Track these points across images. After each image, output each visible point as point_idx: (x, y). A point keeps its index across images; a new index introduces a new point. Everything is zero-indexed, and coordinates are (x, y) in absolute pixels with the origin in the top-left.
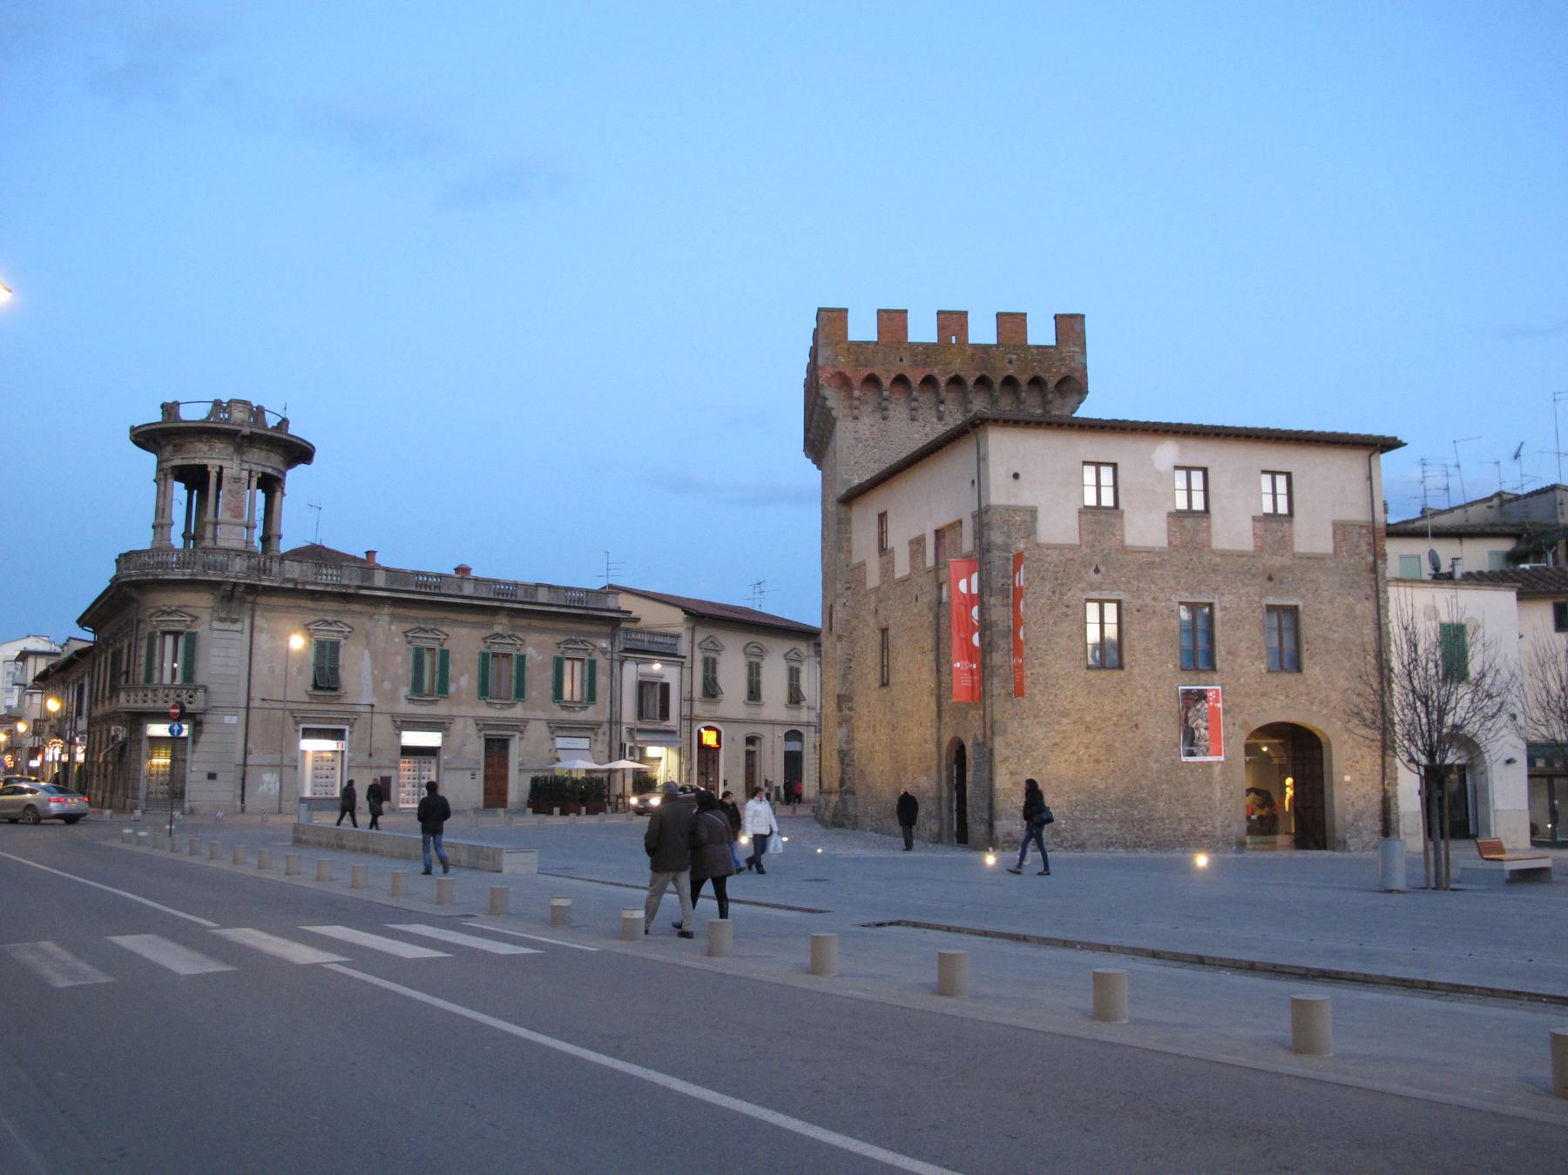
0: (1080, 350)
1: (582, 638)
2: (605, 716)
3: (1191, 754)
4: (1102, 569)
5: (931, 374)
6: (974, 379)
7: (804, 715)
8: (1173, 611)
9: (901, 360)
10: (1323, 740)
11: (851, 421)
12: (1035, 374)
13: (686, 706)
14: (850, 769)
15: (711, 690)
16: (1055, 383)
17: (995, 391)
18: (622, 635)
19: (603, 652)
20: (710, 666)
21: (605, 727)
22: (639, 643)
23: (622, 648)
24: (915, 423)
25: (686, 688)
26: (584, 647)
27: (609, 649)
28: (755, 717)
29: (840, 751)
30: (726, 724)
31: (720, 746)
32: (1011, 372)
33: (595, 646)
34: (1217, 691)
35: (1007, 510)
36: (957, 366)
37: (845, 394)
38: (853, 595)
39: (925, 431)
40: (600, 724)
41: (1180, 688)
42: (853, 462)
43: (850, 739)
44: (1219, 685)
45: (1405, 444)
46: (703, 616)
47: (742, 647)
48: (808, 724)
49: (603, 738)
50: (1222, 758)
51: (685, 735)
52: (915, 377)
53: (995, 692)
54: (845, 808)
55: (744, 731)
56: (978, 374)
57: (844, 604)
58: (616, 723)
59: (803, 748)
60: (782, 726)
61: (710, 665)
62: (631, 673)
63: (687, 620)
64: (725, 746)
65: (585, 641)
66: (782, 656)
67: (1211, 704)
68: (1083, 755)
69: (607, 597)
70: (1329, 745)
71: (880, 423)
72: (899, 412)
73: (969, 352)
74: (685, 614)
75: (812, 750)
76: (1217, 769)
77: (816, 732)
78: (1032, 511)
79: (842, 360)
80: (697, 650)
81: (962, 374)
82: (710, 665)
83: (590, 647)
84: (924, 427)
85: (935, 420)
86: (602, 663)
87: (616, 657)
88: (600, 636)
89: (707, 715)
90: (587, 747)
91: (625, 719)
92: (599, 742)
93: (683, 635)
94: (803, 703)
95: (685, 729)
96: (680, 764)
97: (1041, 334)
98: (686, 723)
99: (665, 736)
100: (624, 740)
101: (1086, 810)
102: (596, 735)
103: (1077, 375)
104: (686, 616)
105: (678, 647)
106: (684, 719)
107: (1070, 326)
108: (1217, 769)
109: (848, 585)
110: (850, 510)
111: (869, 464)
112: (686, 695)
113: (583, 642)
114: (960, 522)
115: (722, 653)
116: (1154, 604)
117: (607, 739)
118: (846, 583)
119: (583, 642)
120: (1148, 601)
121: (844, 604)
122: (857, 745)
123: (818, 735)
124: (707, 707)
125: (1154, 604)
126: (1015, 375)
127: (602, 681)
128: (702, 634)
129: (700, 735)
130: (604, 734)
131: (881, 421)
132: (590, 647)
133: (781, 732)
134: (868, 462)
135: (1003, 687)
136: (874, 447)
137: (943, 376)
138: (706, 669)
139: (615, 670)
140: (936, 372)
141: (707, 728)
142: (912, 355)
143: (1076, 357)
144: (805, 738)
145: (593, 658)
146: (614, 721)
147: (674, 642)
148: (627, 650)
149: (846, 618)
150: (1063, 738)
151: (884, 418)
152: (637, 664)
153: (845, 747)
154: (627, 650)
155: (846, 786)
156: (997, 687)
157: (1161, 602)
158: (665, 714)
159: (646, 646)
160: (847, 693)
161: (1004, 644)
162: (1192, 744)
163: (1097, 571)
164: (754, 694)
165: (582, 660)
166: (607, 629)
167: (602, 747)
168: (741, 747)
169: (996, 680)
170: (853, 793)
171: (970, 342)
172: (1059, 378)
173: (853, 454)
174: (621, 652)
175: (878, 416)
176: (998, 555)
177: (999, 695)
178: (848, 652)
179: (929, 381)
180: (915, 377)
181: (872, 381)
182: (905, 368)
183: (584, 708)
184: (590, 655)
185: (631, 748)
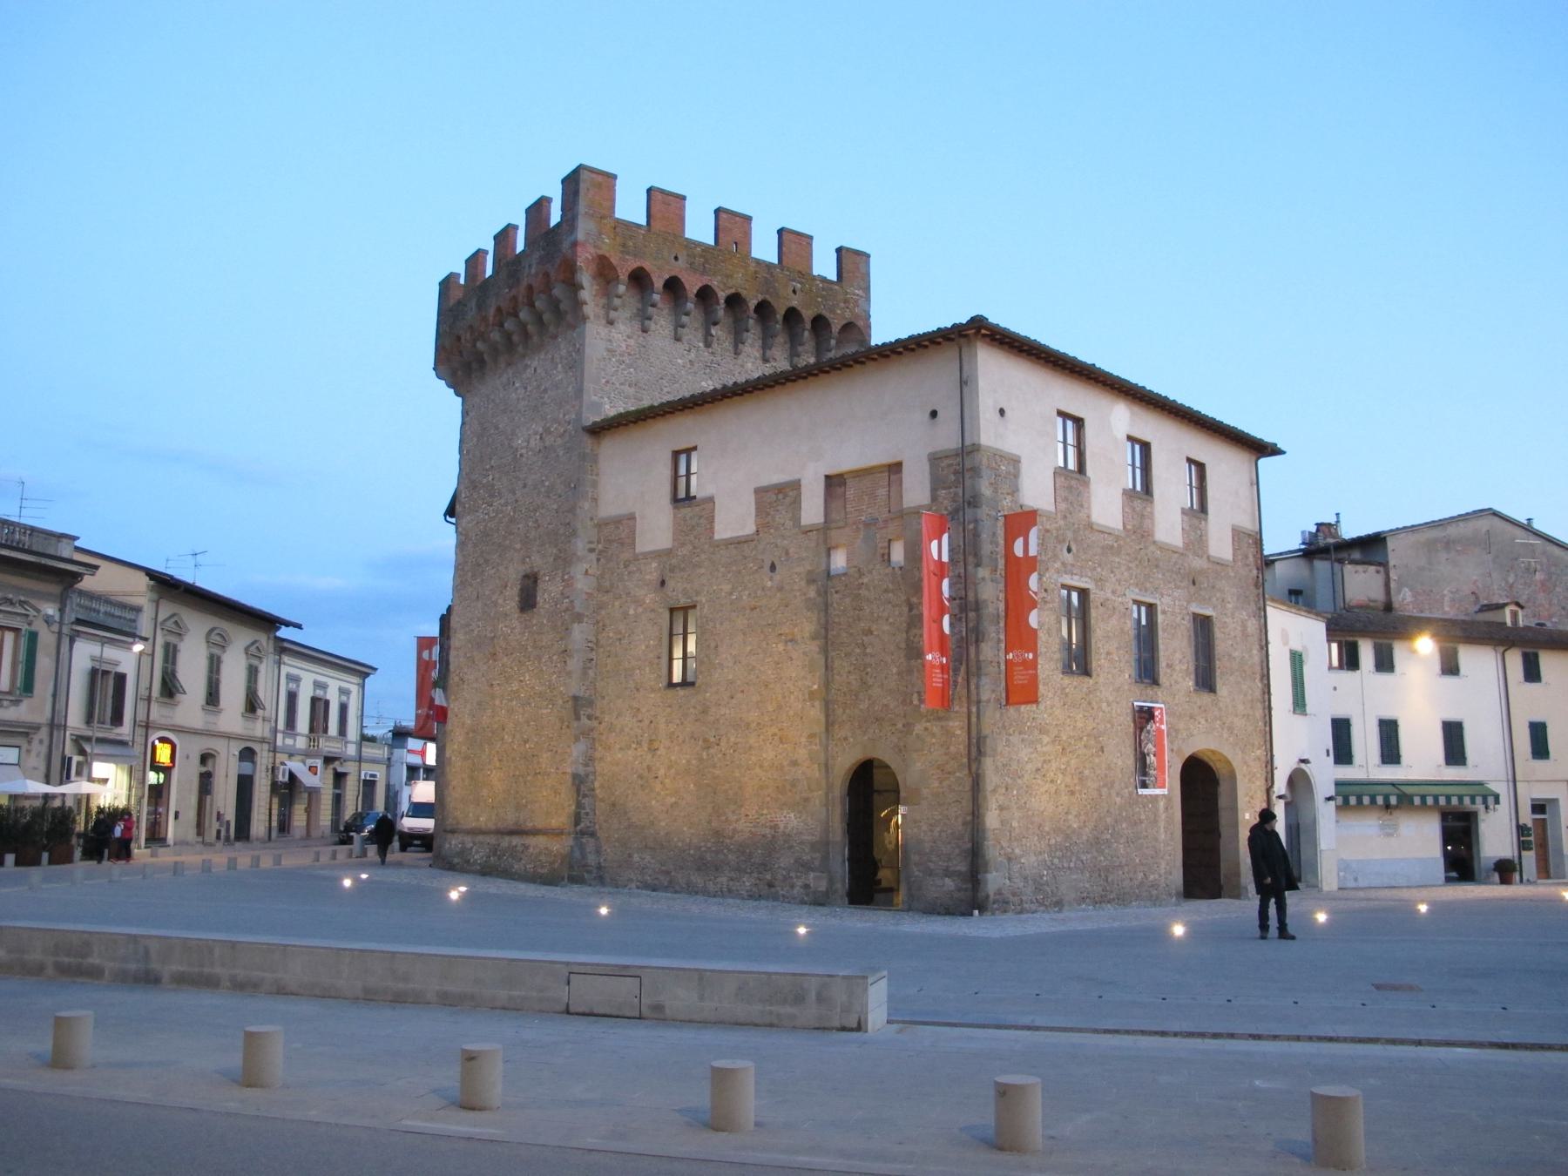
0: (864, 295)
1: (22, 598)
2: (43, 717)
3: (1144, 785)
4: (1074, 548)
5: (709, 284)
6: (755, 302)
7: (259, 729)
8: (1127, 609)
9: (676, 258)
10: (1218, 767)
11: (605, 327)
12: (819, 312)
13: (142, 706)
14: (586, 801)
15: (170, 688)
16: (839, 327)
17: (777, 322)
18: (76, 599)
19: (48, 620)
20: (171, 653)
21: (44, 733)
22: (94, 615)
23: (73, 619)
24: (678, 345)
25: (144, 684)
26: (23, 612)
27: (57, 618)
28: (212, 728)
29: (575, 776)
30: (187, 737)
31: (174, 766)
32: (794, 303)
33: (38, 611)
34: (1161, 709)
35: (995, 455)
36: (738, 282)
37: (598, 288)
38: (598, 560)
39: (690, 358)
40: (37, 728)
41: (1136, 704)
42: (604, 381)
43: (589, 760)
44: (1163, 703)
45: (1284, 453)
46: (166, 586)
47: (204, 635)
48: (262, 741)
49: (39, 748)
50: (1165, 791)
51: (138, 749)
52: (692, 285)
53: (984, 697)
54: (584, 856)
55: (198, 746)
56: (760, 298)
57: (587, 571)
58: (59, 726)
59: (254, 770)
60: (241, 741)
61: (171, 650)
62: (85, 653)
63: (152, 589)
64: (179, 766)
65: (25, 602)
66: (242, 651)
67: (1158, 725)
68: (1060, 784)
69: (59, 541)
70: (1232, 777)
71: (639, 336)
72: (661, 326)
73: (752, 268)
74: (151, 579)
75: (264, 774)
76: (1162, 804)
77: (269, 751)
78: (1015, 461)
79: (607, 241)
80: (159, 632)
81: (744, 293)
82: (171, 650)
83: (32, 612)
84: (689, 351)
85: (701, 345)
86: (46, 638)
87: (65, 630)
88: (47, 597)
89: (163, 721)
90: (17, 762)
91: (70, 723)
92: (33, 754)
93: (145, 608)
94: (260, 712)
95: (140, 740)
96: (130, 789)
97: (824, 266)
98: (140, 731)
99: (115, 748)
100: (68, 752)
101: (1063, 856)
102: (29, 742)
103: (860, 323)
104: (152, 583)
105: (139, 624)
106: (139, 726)
107: (851, 262)
108: (1162, 804)
109: (592, 546)
110: (599, 443)
111: (622, 387)
112: (143, 692)
113: (22, 603)
114: (895, 468)
115: (184, 637)
116: (1113, 598)
117: (44, 749)
118: (590, 542)
119: (22, 603)
120: (1109, 595)
121: (587, 571)
122: (599, 767)
123: (271, 754)
124: (165, 711)
125: (1113, 598)
126: (799, 308)
127: (44, 663)
128: (166, 610)
129: (154, 748)
130: (41, 742)
131: (640, 332)
132: (32, 612)
133: (236, 748)
134: (621, 384)
135: (993, 691)
136: (630, 366)
137: (723, 291)
138: (166, 660)
139: (62, 650)
140: (715, 283)
141: (163, 740)
142: (688, 255)
143: (860, 302)
144: (258, 759)
145: (33, 628)
146: (56, 725)
147: (133, 617)
148: (79, 622)
149: (590, 591)
150: (1045, 761)
151: (645, 330)
152: (102, 645)
153: (581, 770)
154: (79, 622)
155: (582, 825)
156: (990, 689)
157: (1118, 597)
158: (117, 719)
159: (101, 618)
160: (587, 695)
161: (995, 633)
162: (1145, 774)
163: (1069, 550)
164: (213, 697)
165: (16, 630)
166: (55, 589)
167: (37, 761)
168: (195, 769)
169: (985, 681)
170: (593, 834)
171: (753, 255)
172: (844, 322)
173: (604, 370)
174: (73, 623)
175: (637, 325)
176: (987, 512)
177: (989, 701)
178: (589, 638)
179: (705, 294)
180: (692, 285)
181: (639, 279)
182: (680, 269)
183: (16, 702)
184: (30, 624)
185: (79, 764)
